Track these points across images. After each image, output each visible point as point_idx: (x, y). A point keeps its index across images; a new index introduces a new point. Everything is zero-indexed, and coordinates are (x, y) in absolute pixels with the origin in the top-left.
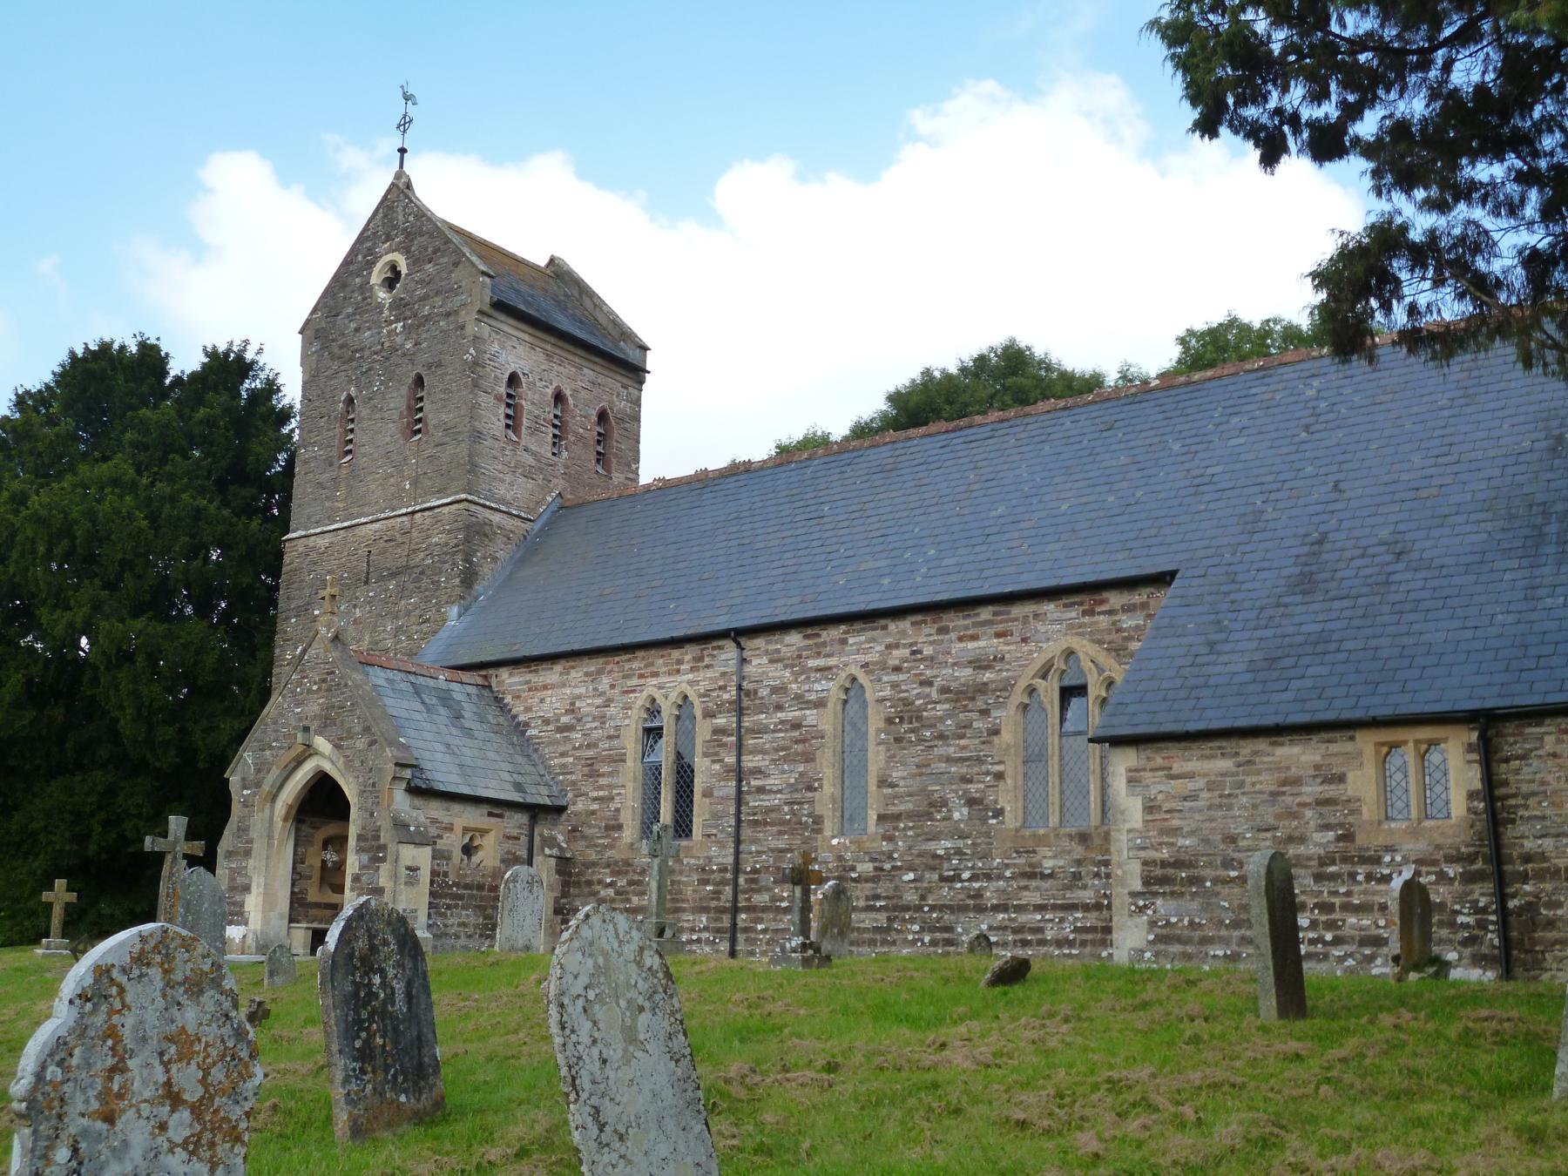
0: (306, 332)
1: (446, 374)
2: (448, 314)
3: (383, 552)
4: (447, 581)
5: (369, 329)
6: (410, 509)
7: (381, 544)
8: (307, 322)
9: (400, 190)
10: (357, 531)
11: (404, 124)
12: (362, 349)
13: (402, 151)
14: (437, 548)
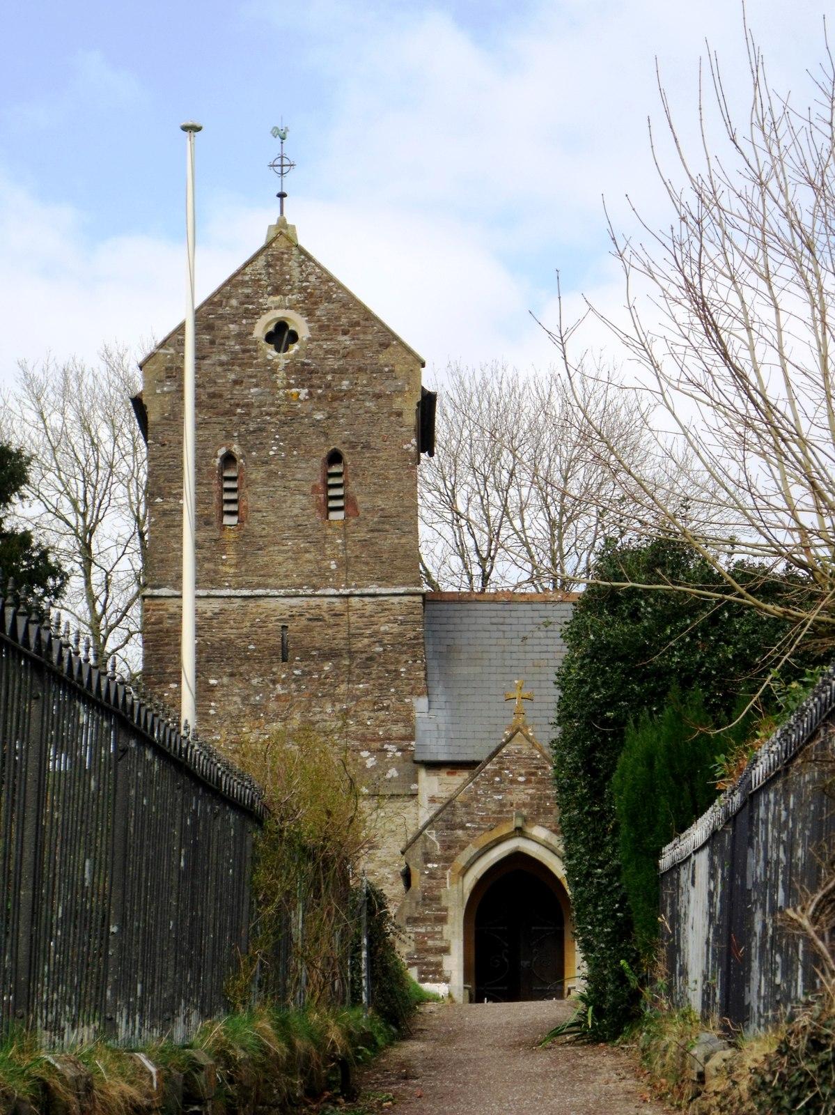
0: (151, 367)
1: (379, 458)
2: (378, 396)
3: (308, 630)
4: (408, 671)
5: (256, 386)
6: (347, 592)
7: (304, 622)
8: (151, 357)
9: (282, 236)
10: (261, 602)
11: (282, 166)
12: (247, 405)
13: (282, 196)
14: (388, 637)
